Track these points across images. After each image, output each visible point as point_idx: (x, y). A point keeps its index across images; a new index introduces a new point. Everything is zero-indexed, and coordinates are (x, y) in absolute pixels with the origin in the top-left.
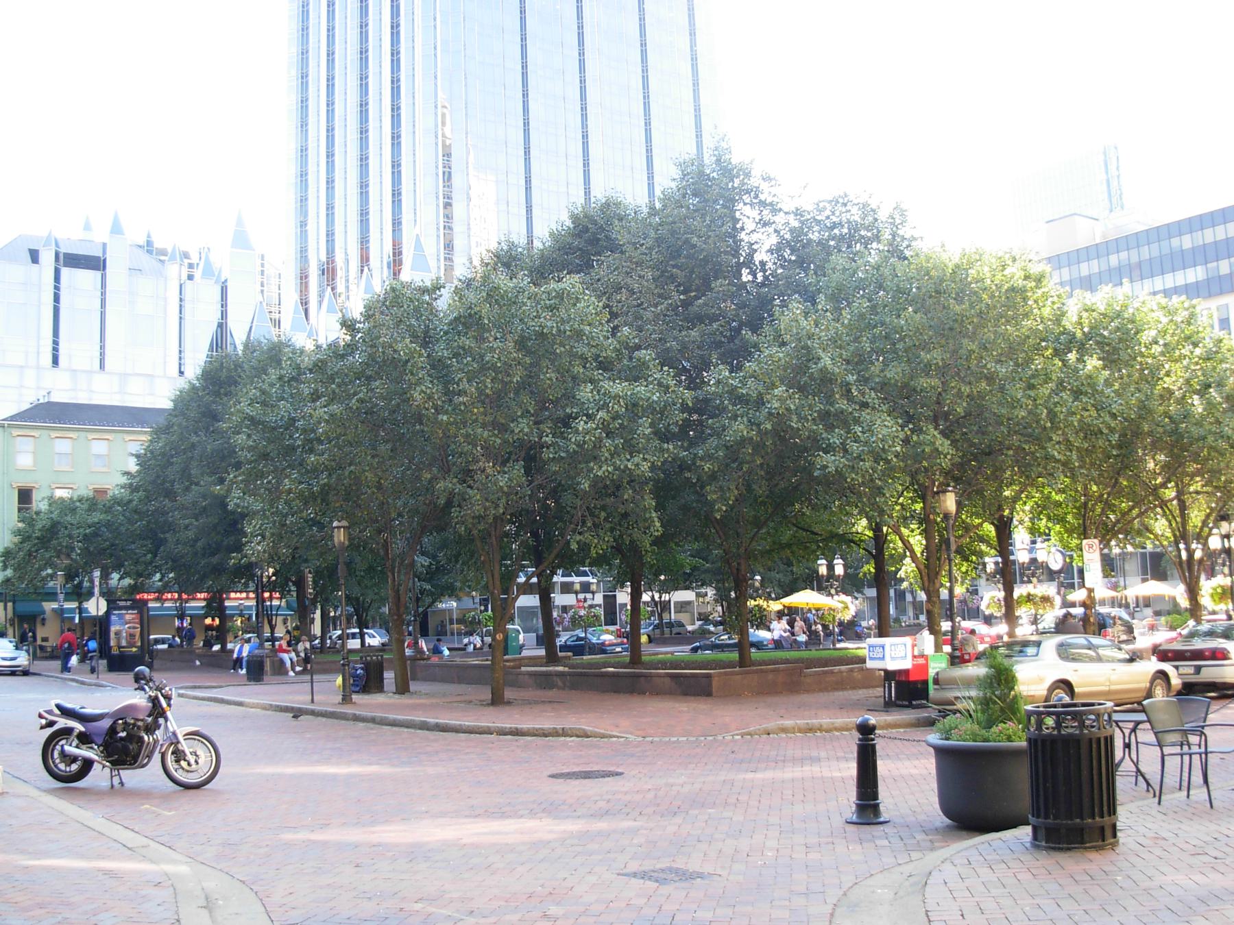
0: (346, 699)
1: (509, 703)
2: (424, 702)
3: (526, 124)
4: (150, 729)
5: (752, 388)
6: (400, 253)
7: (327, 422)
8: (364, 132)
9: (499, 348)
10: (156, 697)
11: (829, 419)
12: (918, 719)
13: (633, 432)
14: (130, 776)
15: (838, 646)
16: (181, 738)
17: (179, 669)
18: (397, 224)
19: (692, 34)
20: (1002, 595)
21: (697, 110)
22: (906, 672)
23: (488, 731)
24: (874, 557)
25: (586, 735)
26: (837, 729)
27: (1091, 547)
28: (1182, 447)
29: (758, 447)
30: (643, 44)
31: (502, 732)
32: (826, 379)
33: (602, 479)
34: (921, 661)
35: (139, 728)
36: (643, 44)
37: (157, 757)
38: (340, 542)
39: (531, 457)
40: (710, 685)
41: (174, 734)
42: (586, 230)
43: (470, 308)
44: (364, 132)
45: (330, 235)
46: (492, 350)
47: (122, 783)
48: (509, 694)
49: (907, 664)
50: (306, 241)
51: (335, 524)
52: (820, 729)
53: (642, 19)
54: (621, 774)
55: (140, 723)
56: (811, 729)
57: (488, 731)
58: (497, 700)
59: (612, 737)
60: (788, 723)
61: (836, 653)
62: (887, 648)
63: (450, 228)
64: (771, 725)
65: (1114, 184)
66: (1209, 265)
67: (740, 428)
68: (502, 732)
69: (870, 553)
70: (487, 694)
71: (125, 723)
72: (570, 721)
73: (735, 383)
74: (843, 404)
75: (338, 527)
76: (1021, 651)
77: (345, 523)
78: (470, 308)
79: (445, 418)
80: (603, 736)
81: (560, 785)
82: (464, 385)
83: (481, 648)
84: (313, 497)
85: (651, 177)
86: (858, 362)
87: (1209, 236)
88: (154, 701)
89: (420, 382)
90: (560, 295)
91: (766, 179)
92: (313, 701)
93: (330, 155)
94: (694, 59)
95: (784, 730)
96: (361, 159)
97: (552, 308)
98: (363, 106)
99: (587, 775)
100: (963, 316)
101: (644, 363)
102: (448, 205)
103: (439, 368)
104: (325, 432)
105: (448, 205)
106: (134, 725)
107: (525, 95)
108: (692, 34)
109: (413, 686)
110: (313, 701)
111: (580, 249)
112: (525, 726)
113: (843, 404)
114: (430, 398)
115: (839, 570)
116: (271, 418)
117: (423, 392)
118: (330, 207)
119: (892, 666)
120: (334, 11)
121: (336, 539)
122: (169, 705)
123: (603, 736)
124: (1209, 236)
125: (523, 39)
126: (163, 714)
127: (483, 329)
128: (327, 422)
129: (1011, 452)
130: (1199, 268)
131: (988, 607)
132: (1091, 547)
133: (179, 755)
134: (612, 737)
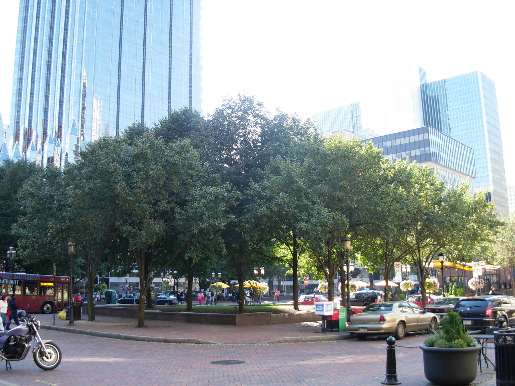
0: (71, 323)
1: (146, 327)
2: (101, 324)
3: (119, 76)
4: (27, 341)
5: (267, 193)
6: (61, 127)
7: (73, 197)
8: (48, 74)
9: (155, 169)
10: (31, 326)
11: (304, 208)
12: (340, 337)
13: (217, 209)
14: (15, 364)
15: (262, 303)
16: (44, 346)
17: (266, 327)
18: (61, 114)
19: (191, 44)
20: (327, 284)
21: (191, 76)
22: (331, 316)
23: (152, 340)
24: (292, 267)
25: (199, 343)
26: (308, 341)
27: (398, 265)
28: (281, 225)
29: (269, 218)
30: (170, 47)
31: (159, 341)
32: (299, 190)
33: (203, 229)
34: (336, 312)
35: (23, 340)
36: (170, 47)
37: (30, 354)
38: (71, 252)
39: (167, 217)
40: (235, 320)
41: (40, 343)
42: (178, 121)
43: (142, 150)
44: (48, 74)
45: (30, 117)
46: (153, 169)
47: (10, 367)
48: (146, 323)
49: (331, 313)
50: (19, 119)
51: (69, 244)
52: (301, 341)
53: (171, 36)
54: (242, 362)
55: (23, 338)
56: (297, 341)
57: (152, 340)
58: (141, 325)
59: (211, 343)
60: (288, 338)
61: (260, 307)
62: (325, 306)
63: (84, 118)
64: (281, 339)
65: (355, 119)
66: (407, 152)
67: (264, 209)
68: (159, 341)
69: (291, 265)
70: (136, 322)
71: (15, 338)
72: (186, 336)
73: (260, 190)
74: (305, 202)
75: (71, 245)
76: (378, 309)
77: (74, 244)
78: (142, 150)
79: (131, 198)
80: (207, 343)
81: (216, 366)
82: (139, 184)
83: (100, 300)
84: (62, 231)
85: (170, 102)
86: (312, 183)
87: (398, 142)
88: (30, 327)
89: (119, 181)
90: (182, 147)
91: (259, 105)
92: (54, 324)
93: (33, 82)
94: (191, 55)
95: (286, 341)
96: (47, 85)
97: (178, 153)
98: (49, 63)
99: (228, 363)
100: (356, 167)
101: (215, 179)
102: (84, 108)
103: (128, 177)
104: (72, 202)
105: (84, 108)
106: (20, 339)
107: (120, 64)
108: (191, 44)
109: (96, 318)
110: (54, 324)
111: (174, 129)
112: (170, 338)
113: (305, 202)
114: (124, 189)
115: (263, 272)
116: (41, 194)
117: (120, 187)
118: (31, 105)
119: (326, 314)
120: (39, 20)
121: (69, 251)
122: (38, 329)
123: (207, 343)
124: (398, 142)
125: (121, 40)
126: (34, 333)
127: (147, 159)
128: (73, 197)
129: (371, 225)
130: (394, 155)
131: (320, 289)
132: (398, 265)
133: (42, 354)
134: (211, 343)
